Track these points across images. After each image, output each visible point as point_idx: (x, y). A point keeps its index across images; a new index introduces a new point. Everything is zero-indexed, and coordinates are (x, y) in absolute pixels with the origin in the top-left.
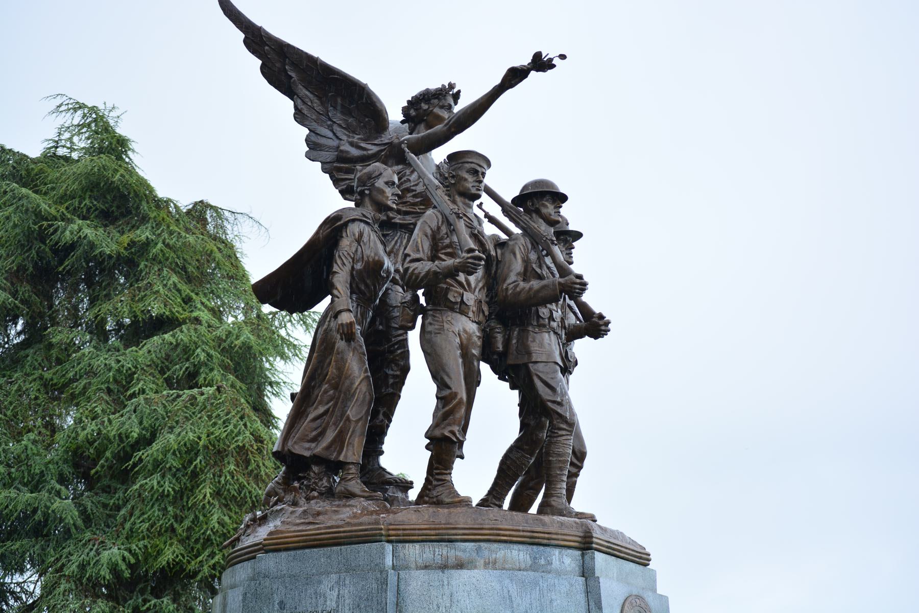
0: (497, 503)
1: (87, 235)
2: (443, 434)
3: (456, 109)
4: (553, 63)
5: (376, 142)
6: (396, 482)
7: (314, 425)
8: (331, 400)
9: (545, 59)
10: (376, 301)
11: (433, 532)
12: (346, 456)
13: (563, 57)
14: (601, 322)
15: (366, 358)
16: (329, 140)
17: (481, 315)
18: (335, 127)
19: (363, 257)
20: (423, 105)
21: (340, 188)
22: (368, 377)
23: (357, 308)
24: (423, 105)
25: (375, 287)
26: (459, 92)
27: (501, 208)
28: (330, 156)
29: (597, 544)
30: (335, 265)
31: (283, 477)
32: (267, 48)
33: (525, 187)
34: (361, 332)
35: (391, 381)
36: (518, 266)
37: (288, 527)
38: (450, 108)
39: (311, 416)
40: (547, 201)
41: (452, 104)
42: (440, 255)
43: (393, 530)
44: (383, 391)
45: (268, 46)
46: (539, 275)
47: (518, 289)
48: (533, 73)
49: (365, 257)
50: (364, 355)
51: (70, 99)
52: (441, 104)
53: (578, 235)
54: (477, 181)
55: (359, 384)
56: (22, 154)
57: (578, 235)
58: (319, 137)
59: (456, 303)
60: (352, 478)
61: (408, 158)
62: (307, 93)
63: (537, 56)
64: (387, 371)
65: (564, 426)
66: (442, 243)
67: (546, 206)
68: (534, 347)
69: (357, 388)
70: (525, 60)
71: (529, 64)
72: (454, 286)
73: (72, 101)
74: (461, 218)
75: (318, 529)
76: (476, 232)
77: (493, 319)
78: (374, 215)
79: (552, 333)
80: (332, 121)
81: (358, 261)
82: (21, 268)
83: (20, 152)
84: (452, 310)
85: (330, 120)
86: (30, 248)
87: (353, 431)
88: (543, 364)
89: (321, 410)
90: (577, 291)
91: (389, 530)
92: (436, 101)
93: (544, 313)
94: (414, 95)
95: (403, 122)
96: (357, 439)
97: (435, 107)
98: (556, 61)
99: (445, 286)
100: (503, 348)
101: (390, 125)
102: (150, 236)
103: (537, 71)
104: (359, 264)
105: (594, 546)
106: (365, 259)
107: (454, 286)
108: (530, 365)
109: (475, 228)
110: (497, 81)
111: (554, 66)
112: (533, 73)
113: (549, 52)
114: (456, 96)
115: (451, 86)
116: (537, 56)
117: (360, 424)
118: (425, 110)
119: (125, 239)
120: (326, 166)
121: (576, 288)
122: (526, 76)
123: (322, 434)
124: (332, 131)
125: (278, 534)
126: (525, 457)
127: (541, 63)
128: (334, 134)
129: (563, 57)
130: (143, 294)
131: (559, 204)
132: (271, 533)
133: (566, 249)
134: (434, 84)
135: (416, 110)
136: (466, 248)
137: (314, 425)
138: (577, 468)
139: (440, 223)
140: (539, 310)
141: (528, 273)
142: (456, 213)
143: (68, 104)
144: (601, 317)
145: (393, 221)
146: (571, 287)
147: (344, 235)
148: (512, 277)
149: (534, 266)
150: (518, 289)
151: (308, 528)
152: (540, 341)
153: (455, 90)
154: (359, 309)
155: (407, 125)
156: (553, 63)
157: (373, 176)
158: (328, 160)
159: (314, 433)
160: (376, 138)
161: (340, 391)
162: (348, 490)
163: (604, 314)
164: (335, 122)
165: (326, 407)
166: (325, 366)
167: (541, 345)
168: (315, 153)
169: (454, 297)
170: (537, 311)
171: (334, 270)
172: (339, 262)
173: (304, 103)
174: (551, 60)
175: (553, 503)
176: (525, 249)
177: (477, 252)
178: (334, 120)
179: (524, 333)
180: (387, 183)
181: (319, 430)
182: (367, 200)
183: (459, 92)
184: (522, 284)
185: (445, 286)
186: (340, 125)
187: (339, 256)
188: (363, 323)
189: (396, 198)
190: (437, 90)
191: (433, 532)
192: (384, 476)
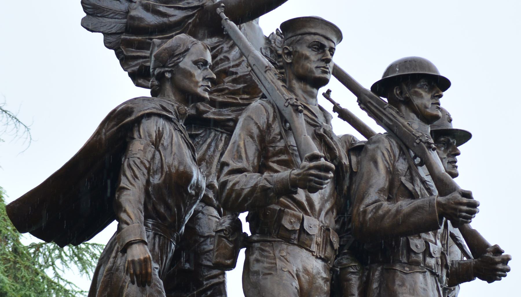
14: (497, 259)
17: (329, 249)
25: (179, 209)
27: (356, 98)
30: (123, 178)
33: (391, 69)
34: (159, 272)
40: (421, 87)
42: (271, 164)
46: (410, 192)
47: (381, 212)
49: (165, 166)
59: (294, 231)
67: (420, 96)
78: (178, 108)
79: (428, 273)
81: (155, 173)
90: (464, 214)
99: (277, 208)
106: (166, 169)
120: (111, 39)
131: (438, 92)
136: (307, 155)
139: (271, 119)
140: (411, 241)
142: (293, 105)
144: (497, 251)
145: (205, 116)
146: (456, 209)
147: (136, 135)
148: (373, 196)
150: (381, 212)
152: (411, 285)
154: (157, 239)
157: (177, 52)
158: (114, 31)
163: (502, 247)
168: (95, 20)
169: (291, 223)
170: (408, 243)
171: (122, 185)
172: (129, 173)
176: (390, 156)
180: (196, 63)
182: (168, 87)
185: (277, 208)
187: (129, 166)
189: (210, 84)
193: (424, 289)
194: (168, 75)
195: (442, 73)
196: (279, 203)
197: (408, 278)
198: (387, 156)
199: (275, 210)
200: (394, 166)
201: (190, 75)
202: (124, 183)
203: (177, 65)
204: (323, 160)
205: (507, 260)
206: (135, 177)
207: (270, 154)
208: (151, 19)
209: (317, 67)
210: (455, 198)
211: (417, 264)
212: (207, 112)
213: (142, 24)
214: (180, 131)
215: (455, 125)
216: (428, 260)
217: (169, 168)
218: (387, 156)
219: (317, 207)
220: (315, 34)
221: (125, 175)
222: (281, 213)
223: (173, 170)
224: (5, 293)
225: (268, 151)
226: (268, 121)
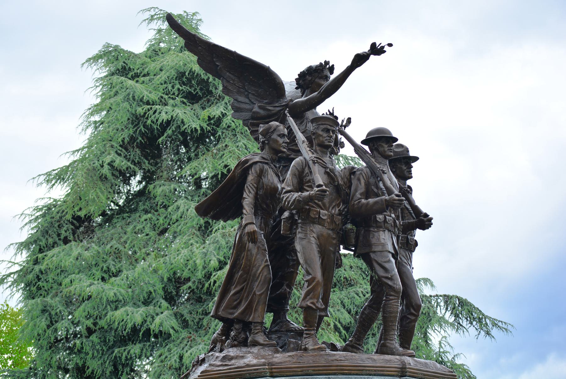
0: (358, 343)
1: (178, 113)
2: (307, 305)
3: (332, 77)
4: (384, 49)
5: (277, 105)
6: (296, 330)
7: (235, 298)
8: (244, 282)
9: (379, 48)
10: (275, 212)
11: (299, 369)
12: (254, 318)
13: (390, 45)
14: (425, 219)
15: (267, 253)
16: (247, 105)
17: (334, 224)
18: (250, 95)
19: (263, 186)
20: (307, 77)
21: (254, 137)
22: (268, 265)
23: (261, 219)
24: (307, 77)
25: (273, 206)
26: (333, 66)
27: (353, 148)
28: (247, 115)
29: (410, 372)
30: (245, 193)
31: (221, 330)
32: (200, 48)
33: (369, 134)
34: (264, 236)
35: (291, 263)
36: (362, 188)
37: (212, 368)
38: (327, 78)
39: (232, 292)
40: (383, 142)
41: (329, 74)
42: (305, 187)
43: (275, 368)
44: (286, 270)
45: (200, 46)
46: (376, 193)
47: (360, 204)
48: (372, 56)
49: (265, 186)
50: (265, 250)
51: (161, 10)
52: (320, 76)
53: (416, 159)
54: (329, 137)
55: (262, 270)
56: (130, 52)
57: (416, 159)
58: (240, 103)
59: (316, 218)
60: (258, 332)
61: (289, 121)
62: (230, 75)
63: (373, 45)
64: (288, 257)
65: (392, 293)
66: (306, 179)
67: (383, 147)
68: (374, 241)
69: (260, 273)
70: (366, 48)
71: (369, 51)
72: (313, 207)
73: (162, 12)
74: (316, 163)
75: (230, 369)
76: (328, 170)
77: (349, 223)
78: (272, 157)
79: (387, 232)
80: (248, 92)
81: (260, 189)
82: (132, 139)
83: (129, 50)
84: (314, 223)
85: (247, 91)
86: (139, 123)
87: (258, 302)
88: (379, 253)
89: (238, 288)
90: (397, 205)
91: (272, 369)
92: (316, 74)
93: (380, 219)
94: (302, 71)
95: (297, 88)
96: (260, 307)
97: (316, 78)
98: (387, 48)
99: (308, 207)
100: (355, 242)
101: (286, 93)
102: (223, 111)
103: (375, 55)
104: (261, 191)
105: (408, 374)
106: (265, 187)
107: (313, 207)
108: (371, 254)
109: (328, 168)
110: (349, 63)
111: (385, 51)
112: (372, 56)
113: (381, 41)
114: (332, 69)
115: (327, 63)
116: (373, 45)
117: (263, 296)
118: (310, 81)
119: (205, 114)
120: (246, 122)
121: (395, 203)
122: (368, 59)
123: (239, 304)
124: (248, 98)
125: (206, 373)
126: (375, 313)
127: (376, 50)
128: (250, 100)
129: (390, 45)
130: (222, 153)
131: (391, 144)
132: (202, 372)
133: (407, 168)
134: (315, 62)
135: (303, 81)
136: (316, 184)
137: (235, 298)
138: (414, 316)
139: (304, 166)
140: (377, 216)
141: (368, 194)
142: (312, 160)
143: (159, 14)
144: (426, 215)
145: (290, 157)
146: (393, 203)
147: (250, 172)
148: (358, 195)
149: (373, 187)
150: (360, 204)
151: (225, 368)
152: (377, 237)
153: (331, 65)
154: (263, 220)
155: (300, 90)
156: (384, 49)
157: (271, 131)
158: (247, 118)
159: (235, 303)
160: (277, 102)
161: (250, 275)
162: (255, 340)
163: (428, 214)
164: (250, 93)
165: (242, 286)
166: (241, 259)
167: (379, 239)
168: (238, 114)
169: (314, 214)
170: (376, 217)
171: (244, 196)
172: (247, 191)
173: (228, 82)
174: (383, 47)
175: (388, 344)
176: (366, 178)
177: (324, 186)
178: (250, 91)
179: (368, 232)
180: (279, 135)
181: (238, 301)
182: (267, 147)
183: (333, 66)
184: (363, 201)
185: (308, 207)
186: (253, 94)
187: (247, 187)
188: (265, 229)
189: (286, 145)
190: (317, 66)
191: (299, 369)
192: (289, 325)
193: (384, 239)
194: (266, 142)
195: (394, 135)
196: (308, 205)
197: (376, 234)
198: (365, 177)
199: (306, 209)
200: (368, 181)
201: (277, 141)
202: (245, 195)
203: (270, 137)
204: (324, 186)
205: (431, 219)
206: (250, 192)
207: (304, 183)
208: (262, 112)
209: (326, 140)
210: (393, 197)
211: (381, 227)
212: (291, 155)
213: (258, 115)
214: (272, 168)
215: (412, 154)
216: (386, 224)
217: (267, 187)
218: (365, 177)
219: (327, 206)
220: (325, 124)
221: (245, 191)
222: (309, 210)
223: (268, 187)
224: (347, 174)
225: (303, 181)
226: (303, 167)
